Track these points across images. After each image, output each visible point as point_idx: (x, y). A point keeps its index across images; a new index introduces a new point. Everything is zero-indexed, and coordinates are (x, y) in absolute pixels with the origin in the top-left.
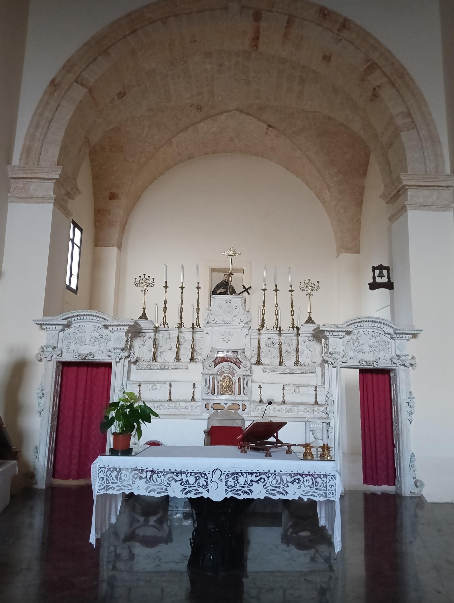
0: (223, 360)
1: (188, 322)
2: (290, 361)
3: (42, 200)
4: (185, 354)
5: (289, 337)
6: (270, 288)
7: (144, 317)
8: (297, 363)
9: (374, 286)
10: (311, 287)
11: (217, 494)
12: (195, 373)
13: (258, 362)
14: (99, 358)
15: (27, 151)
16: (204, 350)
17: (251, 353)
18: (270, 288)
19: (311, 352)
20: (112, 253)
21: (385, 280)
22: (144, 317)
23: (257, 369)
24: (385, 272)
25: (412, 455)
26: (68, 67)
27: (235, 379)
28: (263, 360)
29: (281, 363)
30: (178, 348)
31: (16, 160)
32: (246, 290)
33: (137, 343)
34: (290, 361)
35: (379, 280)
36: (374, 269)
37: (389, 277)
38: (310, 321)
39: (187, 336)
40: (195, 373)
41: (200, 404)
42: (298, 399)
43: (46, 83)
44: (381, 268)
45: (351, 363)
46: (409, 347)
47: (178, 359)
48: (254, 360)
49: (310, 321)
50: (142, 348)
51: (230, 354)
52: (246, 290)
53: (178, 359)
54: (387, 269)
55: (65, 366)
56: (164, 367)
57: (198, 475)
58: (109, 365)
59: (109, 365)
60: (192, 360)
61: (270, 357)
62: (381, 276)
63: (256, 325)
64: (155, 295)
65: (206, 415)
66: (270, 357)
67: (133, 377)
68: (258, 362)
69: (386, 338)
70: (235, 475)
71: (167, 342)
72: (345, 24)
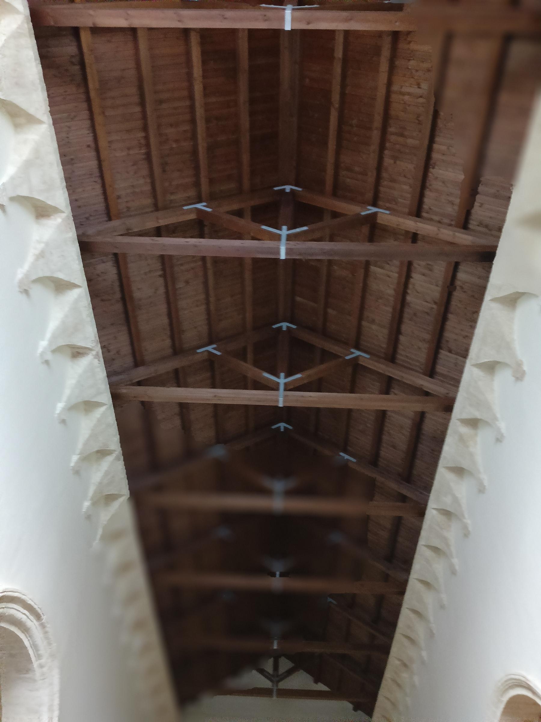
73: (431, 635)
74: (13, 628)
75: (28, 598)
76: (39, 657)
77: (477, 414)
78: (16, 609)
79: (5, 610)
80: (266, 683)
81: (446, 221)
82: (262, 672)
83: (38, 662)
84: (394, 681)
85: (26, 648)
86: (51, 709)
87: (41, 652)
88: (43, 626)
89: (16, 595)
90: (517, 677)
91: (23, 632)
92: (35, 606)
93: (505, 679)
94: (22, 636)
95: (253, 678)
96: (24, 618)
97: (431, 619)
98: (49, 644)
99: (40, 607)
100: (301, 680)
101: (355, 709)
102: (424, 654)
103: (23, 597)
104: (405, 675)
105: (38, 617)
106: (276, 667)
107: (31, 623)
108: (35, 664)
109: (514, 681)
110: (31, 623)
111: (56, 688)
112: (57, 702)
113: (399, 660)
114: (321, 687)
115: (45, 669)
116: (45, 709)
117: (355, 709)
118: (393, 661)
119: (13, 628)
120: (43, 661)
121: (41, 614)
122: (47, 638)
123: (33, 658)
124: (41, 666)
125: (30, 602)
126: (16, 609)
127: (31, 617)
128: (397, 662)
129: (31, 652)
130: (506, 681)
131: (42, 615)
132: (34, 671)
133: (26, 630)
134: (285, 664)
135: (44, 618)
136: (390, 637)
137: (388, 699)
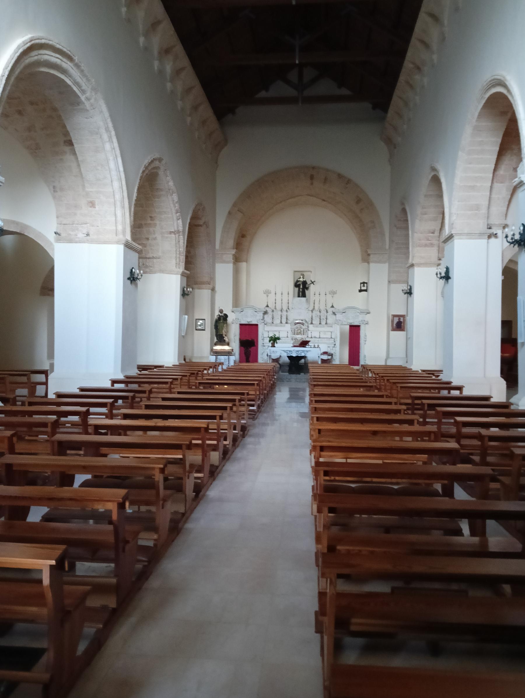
0: (298, 323)
1: (285, 308)
2: (323, 322)
3: (228, 262)
4: (284, 321)
5: (323, 312)
6: (317, 294)
7: (267, 306)
8: (326, 323)
9: (361, 291)
10: (333, 293)
11: (294, 355)
12: (288, 327)
13: (312, 323)
14: (254, 322)
15: (221, 243)
16: (290, 320)
17: (309, 320)
18: (317, 294)
19: (331, 319)
20: (244, 265)
21: (365, 288)
22: (267, 306)
23: (311, 326)
24: (365, 285)
25: (365, 356)
26: (235, 205)
27: (302, 330)
28: (313, 322)
29: (320, 324)
30: (281, 318)
31: (217, 246)
32: (313, 283)
33: (266, 316)
34: (323, 322)
35: (363, 288)
36: (361, 283)
37: (367, 287)
38: (332, 307)
39: (284, 313)
40: (288, 327)
41: (290, 338)
42: (325, 336)
43: (227, 211)
44: (364, 283)
45: (344, 323)
46: (367, 318)
47: (281, 322)
48: (310, 323)
49: (332, 307)
50: (268, 318)
51: (300, 321)
52: (313, 283)
53: (281, 322)
54: (366, 283)
55: (241, 325)
56: (276, 325)
57: (290, 351)
58: (257, 325)
59: (257, 325)
60: (287, 323)
61: (316, 321)
62: (364, 286)
63: (311, 308)
64: (272, 296)
65: (292, 342)
66: (316, 321)
67: (266, 329)
68: (312, 323)
69: (358, 314)
70: (298, 351)
71: (277, 314)
72: (349, 181)
73: (443, 39)
74: (52, 72)
75: (54, 42)
76: (83, 92)
77: (304, 338)
78: (48, 55)
79: (39, 57)
80: (291, 92)
81: (315, 492)
82: (288, 82)
83: (84, 96)
84: (407, 83)
85: (69, 86)
86: (107, 130)
87: (84, 87)
88: (77, 66)
89: (43, 41)
90: (499, 77)
91: (62, 73)
92: (65, 50)
93: (490, 80)
94: (62, 77)
95: (279, 89)
96: (58, 61)
97: (446, 22)
98: (88, 80)
99: (68, 49)
100: (326, 87)
101: (374, 108)
102: (435, 57)
103: (51, 43)
104: (417, 77)
105: (70, 58)
106: (301, 76)
107: (66, 64)
108: (83, 98)
109: (496, 81)
110: (66, 64)
111: (107, 114)
112: (110, 125)
113: (413, 63)
114: (345, 92)
115: (92, 101)
116: (103, 131)
117: (374, 108)
118: (407, 65)
119: (52, 72)
120: (88, 94)
121: (72, 55)
122: (85, 76)
123: (79, 94)
124: (88, 99)
125: (58, 46)
126: (48, 55)
127: (64, 60)
128: (411, 66)
129: (75, 88)
130: (490, 81)
131: (73, 56)
132: (84, 103)
133: (64, 71)
134: (309, 74)
135: (76, 58)
136: (407, 41)
137: (401, 98)
